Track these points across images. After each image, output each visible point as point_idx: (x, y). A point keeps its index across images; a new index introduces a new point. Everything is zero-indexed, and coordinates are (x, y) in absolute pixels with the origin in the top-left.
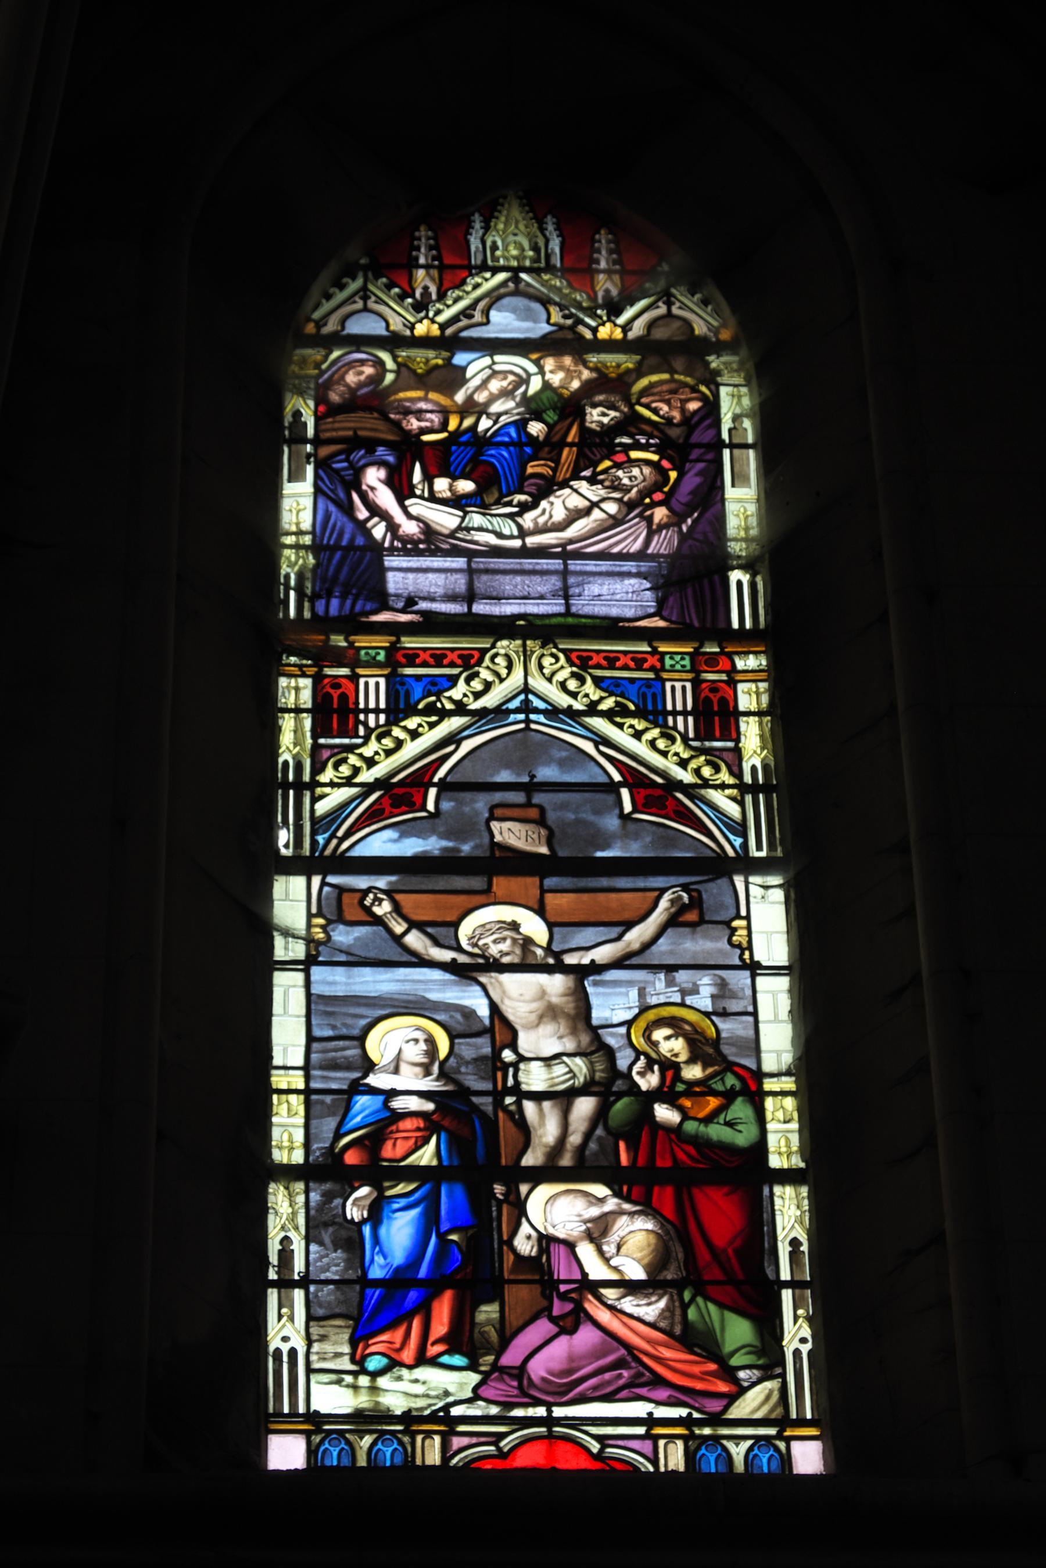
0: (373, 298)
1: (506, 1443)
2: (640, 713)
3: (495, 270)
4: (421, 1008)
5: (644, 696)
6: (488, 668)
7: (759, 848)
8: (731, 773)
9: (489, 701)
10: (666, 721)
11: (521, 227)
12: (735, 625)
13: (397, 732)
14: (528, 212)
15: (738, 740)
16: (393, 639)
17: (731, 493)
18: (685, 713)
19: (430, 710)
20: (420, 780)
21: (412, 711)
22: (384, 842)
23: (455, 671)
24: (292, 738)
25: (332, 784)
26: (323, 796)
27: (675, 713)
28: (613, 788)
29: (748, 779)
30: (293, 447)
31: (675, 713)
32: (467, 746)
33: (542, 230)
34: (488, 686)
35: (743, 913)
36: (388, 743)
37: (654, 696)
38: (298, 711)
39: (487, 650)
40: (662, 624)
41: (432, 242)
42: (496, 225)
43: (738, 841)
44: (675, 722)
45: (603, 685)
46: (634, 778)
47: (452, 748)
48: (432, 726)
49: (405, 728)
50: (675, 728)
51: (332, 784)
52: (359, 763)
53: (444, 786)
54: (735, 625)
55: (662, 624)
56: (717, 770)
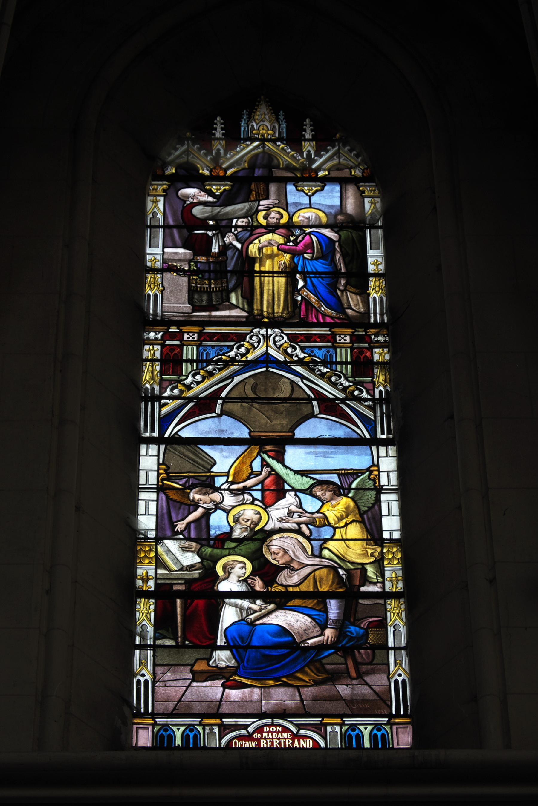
0: (192, 156)
1: (251, 729)
3: (253, 140)
4: (246, 422)
6: (248, 342)
7: (383, 433)
8: (368, 393)
9: (250, 357)
11: (267, 117)
12: (134, 745)
13: (202, 373)
15: (373, 378)
16: (200, 328)
17: (370, 252)
20: (216, 395)
23: (232, 343)
24: (149, 376)
25: (169, 398)
26: (165, 404)
28: (309, 400)
29: (377, 396)
30: (152, 230)
31: (341, 363)
32: (237, 379)
33: (277, 119)
34: (248, 351)
35: (376, 463)
36: (199, 378)
38: (153, 361)
39: (248, 334)
40: (329, 333)
41: (223, 126)
42: (254, 116)
44: (341, 368)
45: (306, 351)
46: (320, 397)
47: (230, 380)
48: (220, 370)
51: (169, 398)
52: (183, 388)
53: (226, 400)
54: (372, 320)
55: (329, 333)
56: (362, 392)
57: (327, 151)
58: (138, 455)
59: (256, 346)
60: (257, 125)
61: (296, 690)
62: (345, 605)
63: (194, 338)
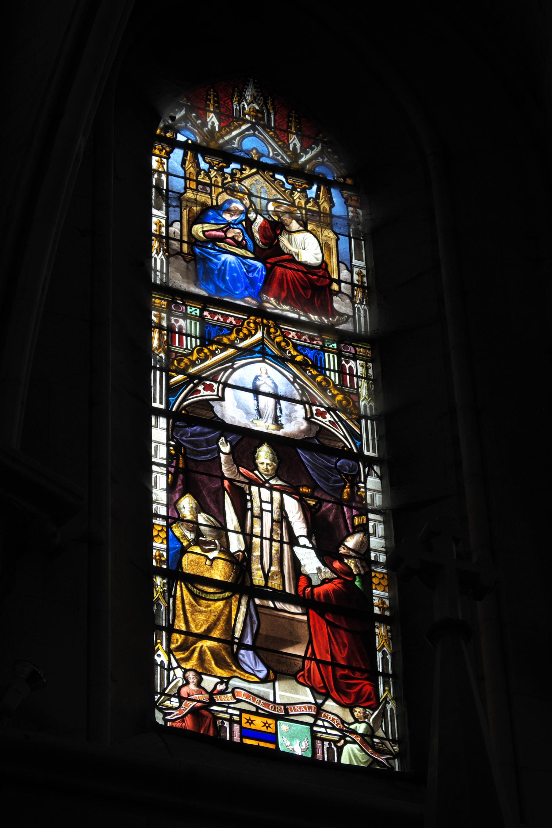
2: (314, 367)
5: (316, 357)
6: (246, 328)
7: (368, 450)
10: (325, 373)
13: (206, 350)
14: (280, 421)
18: (334, 371)
19: (219, 343)
21: (212, 343)
22: (256, 378)
27: (330, 370)
37: (321, 358)
43: (358, 444)
44: (330, 374)
49: (209, 349)
50: (330, 377)
57: (312, 149)
58: (150, 427)
59: (253, 333)
60: (248, 105)
61: (348, 710)
62: (154, 620)
63: (196, 314)
